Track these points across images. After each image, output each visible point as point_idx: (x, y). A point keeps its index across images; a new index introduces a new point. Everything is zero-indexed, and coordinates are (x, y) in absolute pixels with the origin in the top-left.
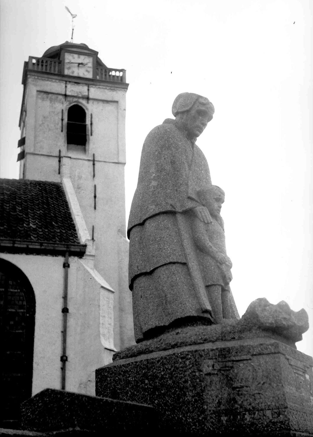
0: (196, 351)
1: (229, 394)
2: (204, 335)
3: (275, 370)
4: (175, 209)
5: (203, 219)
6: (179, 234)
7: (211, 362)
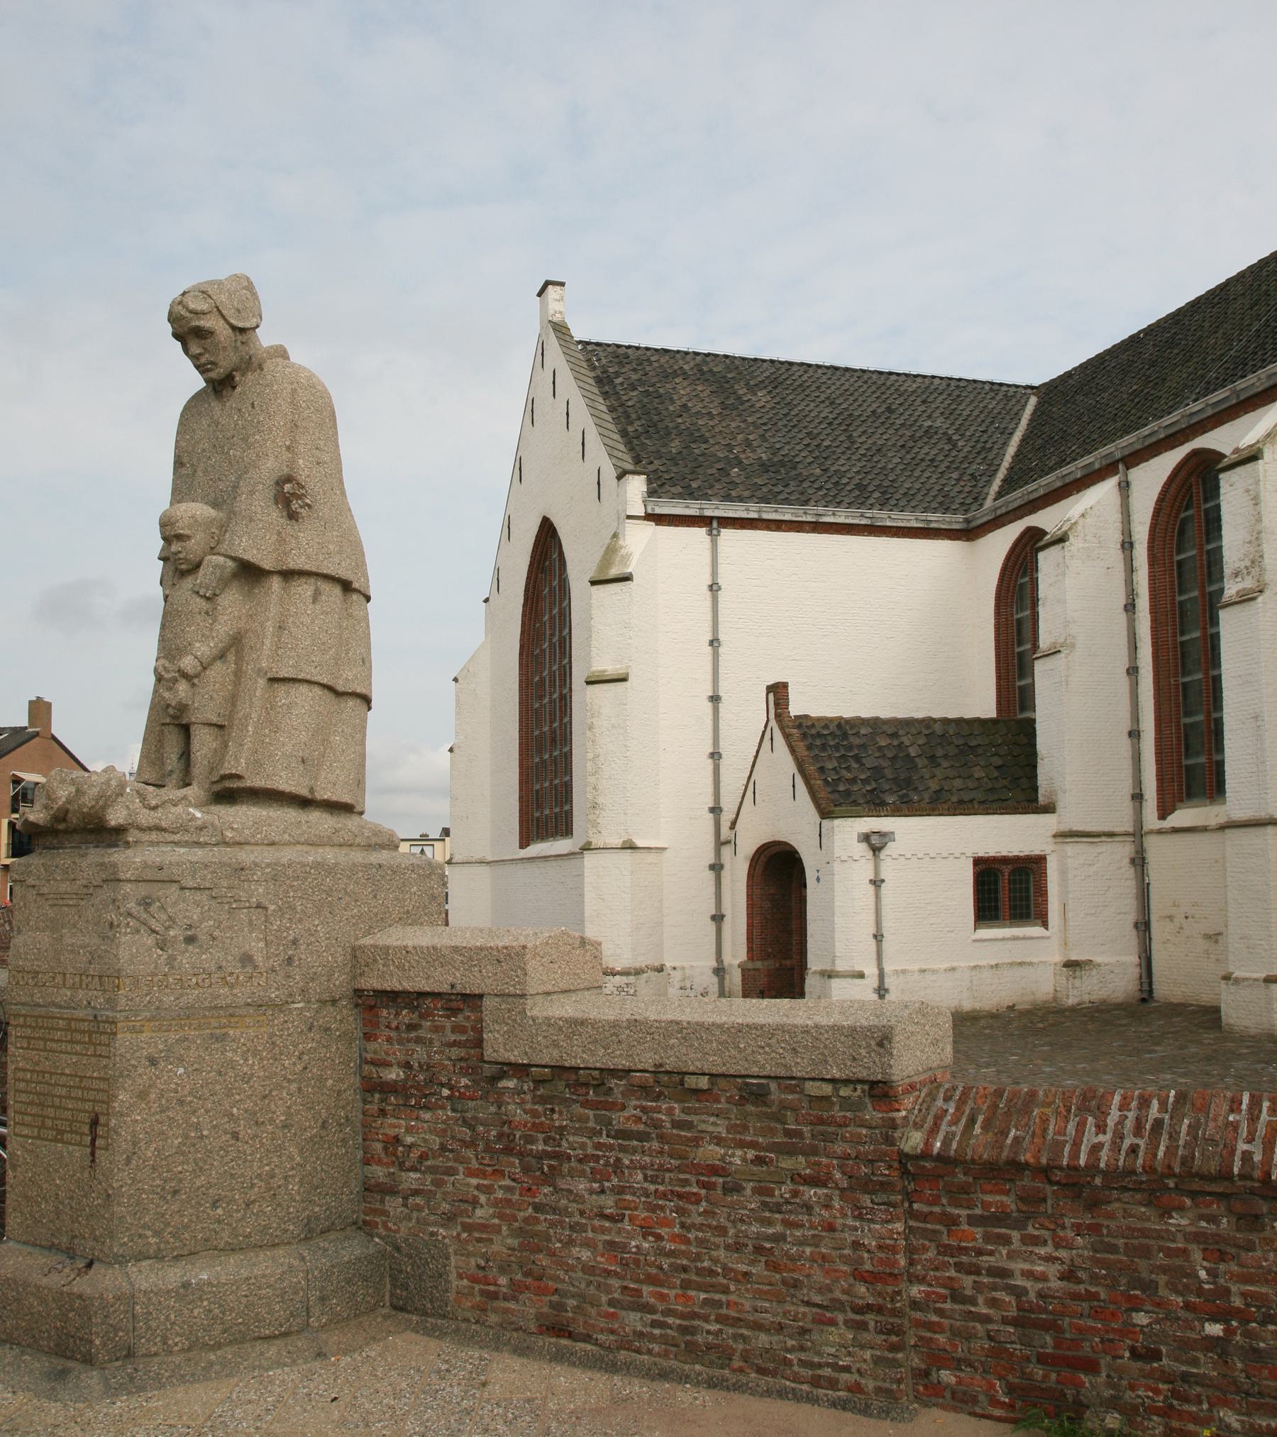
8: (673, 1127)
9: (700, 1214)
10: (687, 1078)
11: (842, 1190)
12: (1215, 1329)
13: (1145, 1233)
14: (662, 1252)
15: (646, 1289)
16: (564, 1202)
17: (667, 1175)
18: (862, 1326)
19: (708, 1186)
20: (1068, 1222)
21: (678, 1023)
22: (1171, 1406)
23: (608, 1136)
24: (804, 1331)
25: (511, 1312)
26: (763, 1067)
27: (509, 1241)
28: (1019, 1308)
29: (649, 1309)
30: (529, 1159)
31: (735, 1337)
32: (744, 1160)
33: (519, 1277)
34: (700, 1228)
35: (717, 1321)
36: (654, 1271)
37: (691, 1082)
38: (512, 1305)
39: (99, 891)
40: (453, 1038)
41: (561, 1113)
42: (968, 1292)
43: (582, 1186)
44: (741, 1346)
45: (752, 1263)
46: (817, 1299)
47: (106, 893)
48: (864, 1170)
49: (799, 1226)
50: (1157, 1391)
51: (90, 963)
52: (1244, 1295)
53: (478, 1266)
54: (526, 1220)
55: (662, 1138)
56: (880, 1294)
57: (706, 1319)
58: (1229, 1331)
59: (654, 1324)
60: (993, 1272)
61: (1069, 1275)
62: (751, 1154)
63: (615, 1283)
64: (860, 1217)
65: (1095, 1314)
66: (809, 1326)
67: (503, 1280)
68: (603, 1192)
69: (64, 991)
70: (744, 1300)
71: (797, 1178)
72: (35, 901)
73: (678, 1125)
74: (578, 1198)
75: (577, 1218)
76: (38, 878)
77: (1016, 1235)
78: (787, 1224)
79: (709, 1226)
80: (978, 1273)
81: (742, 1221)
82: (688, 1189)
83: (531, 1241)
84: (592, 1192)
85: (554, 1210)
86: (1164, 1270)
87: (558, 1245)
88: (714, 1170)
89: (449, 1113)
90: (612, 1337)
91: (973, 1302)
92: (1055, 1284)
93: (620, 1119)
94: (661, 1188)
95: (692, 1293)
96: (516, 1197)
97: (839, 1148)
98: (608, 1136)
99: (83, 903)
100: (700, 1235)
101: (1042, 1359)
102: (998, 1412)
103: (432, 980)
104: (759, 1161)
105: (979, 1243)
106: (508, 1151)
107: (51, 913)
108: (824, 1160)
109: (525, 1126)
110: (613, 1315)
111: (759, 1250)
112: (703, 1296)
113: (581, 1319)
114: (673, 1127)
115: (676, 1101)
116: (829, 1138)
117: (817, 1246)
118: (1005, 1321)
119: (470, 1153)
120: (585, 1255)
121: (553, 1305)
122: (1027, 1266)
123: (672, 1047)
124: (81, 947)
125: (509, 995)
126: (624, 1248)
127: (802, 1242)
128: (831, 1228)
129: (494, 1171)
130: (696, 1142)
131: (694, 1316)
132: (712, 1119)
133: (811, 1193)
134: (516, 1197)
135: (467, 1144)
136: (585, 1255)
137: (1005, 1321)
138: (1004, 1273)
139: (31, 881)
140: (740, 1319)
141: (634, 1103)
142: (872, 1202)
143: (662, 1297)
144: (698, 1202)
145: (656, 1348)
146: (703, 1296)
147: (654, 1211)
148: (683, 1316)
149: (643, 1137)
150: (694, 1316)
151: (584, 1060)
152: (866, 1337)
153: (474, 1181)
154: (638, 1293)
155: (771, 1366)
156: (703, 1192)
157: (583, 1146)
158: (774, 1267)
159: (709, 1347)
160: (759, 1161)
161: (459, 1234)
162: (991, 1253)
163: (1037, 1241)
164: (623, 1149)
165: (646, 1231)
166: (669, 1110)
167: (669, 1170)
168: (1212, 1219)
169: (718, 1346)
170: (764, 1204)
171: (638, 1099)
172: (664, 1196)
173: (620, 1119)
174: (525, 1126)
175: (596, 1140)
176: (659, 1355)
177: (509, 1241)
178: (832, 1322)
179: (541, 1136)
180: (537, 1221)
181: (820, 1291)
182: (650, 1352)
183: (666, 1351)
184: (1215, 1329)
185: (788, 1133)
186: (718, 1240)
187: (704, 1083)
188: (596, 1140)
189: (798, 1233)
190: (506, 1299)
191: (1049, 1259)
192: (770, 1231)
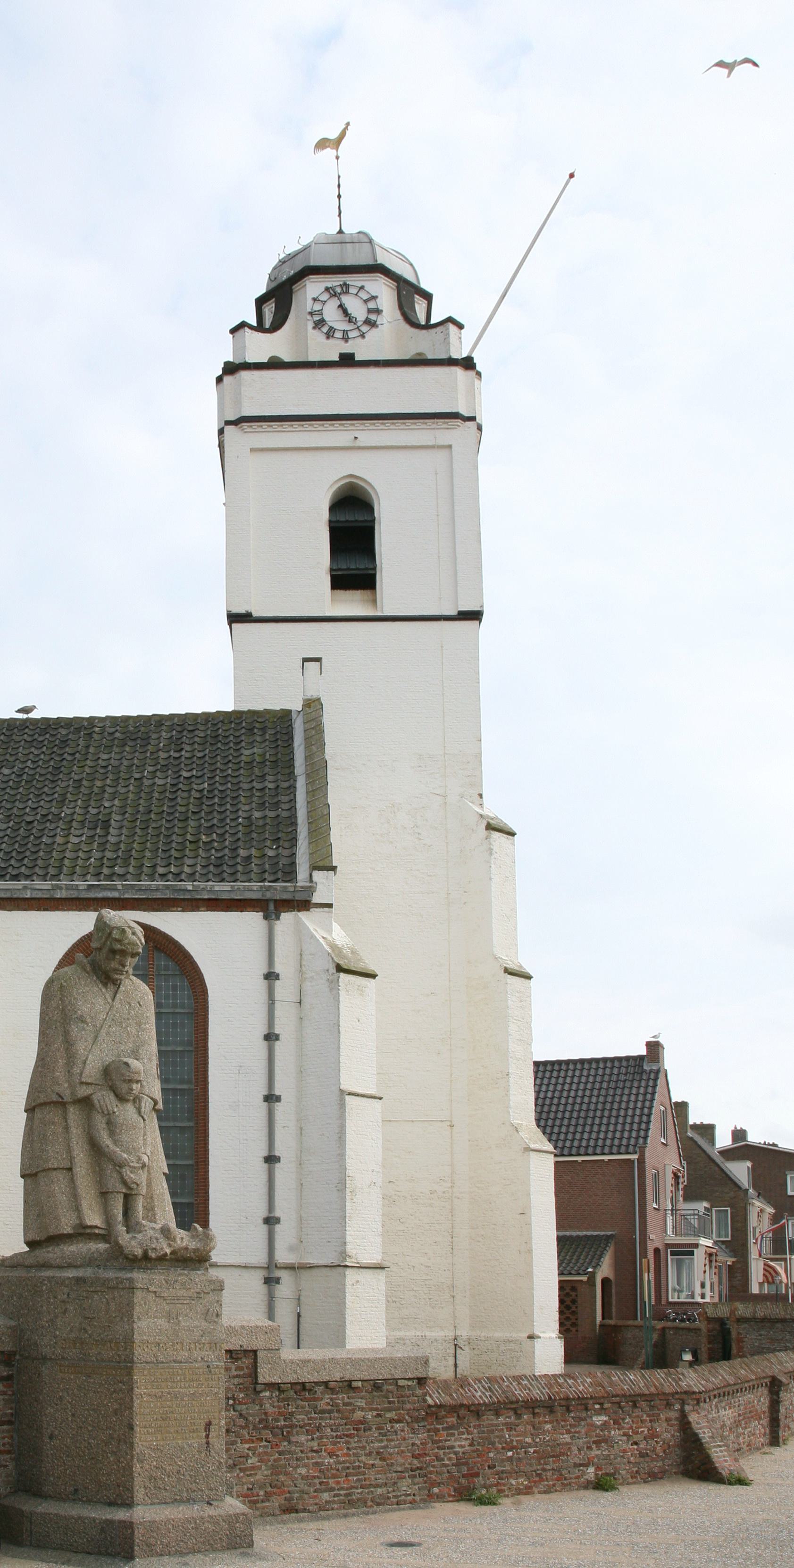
0: (53, 1277)
1: (80, 1324)
2: (69, 1259)
3: (128, 1305)
4: (63, 1099)
5: (102, 1109)
6: (67, 1128)
7: (66, 1290)
8: (344, 1405)
9: (355, 1442)
10: (353, 1383)
11: (408, 1423)
12: (510, 1454)
13: (492, 1425)
14: (339, 1462)
15: (331, 1481)
16: (294, 1448)
17: (341, 1427)
18: (415, 1476)
19: (357, 1430)
20: (472, 1425)
21: (350, 1359)
22: (498, 1483)
23: (315, 1413)
24: (395, 1483)
25: (267, 1507)
26: (384, 1376)
27: (265, 1472)
28: (457, 1459)
29: (332, 1489)
30: (276, 1430)
31: (368, 1493)
32: (372, 1416)
33: (269, 1489)
34: (355, 1448)
35: (361, 1488)
36: (334, 1472)
37: (354, 1384)
38: (267, 1504)
39: (207, 1296)
40: (235, 1373)
41: (292, 1405)
42: (442, 1456)
43: (303, 1438)
44: (370, 1496)
45: (375, 1459)
46: (400, 1469)
47: (212, 1297)
48: (417, 1414)
49: (392, 1440)
50: (495, 1478)
51: (202, 1336)
52: (517, 1441)
53: (248, 1489)
54: (275, 1460)
55: (338, 1411)
56: (422, 1462)
57: (357, 1488)
58: (513, 1454)
59: (335, 1496)
60: (449, 1448)
61: (471, 1445)
62: (375, 1413)
63: (317, 1481)
64: (414, 1433)
65: (479, 1456)
66: (396, 1481)
67: (262, 1493)
68: (313, 1439)
69: (182, 1353)
70: (371, 1475)
71: (392, 1421)
72: (155, 1301)
73: (345, 1404)
74: (302, 1445)
75: (300, 1454)
76: (160, 1287)
77: (456, 1432)
78: (388, 1440)
79: (359, 1447)
80: (444, 1449)
81: (372, 1442)
82: (350, 1432)
83: (276, 1470)
84: (307, 1441)
85: (289, 1452)
86: (497, 1437)
87: (291, 1469)
88: (361, 1422)
89: (232, 1413)
90: (316, 1507)
91: (443, 1460)
92: (467, 1448)
93: (322, 1405)
94: (339, 1434)
95: (350, 1478)
96: (269, 1450)
97: (408, 1406)
98: (315, 1413)
99: (193, 1302)
100: (355, 1451)
101: (464, 1476)
102: (451, 1499)
103: (229, 1344)
104: (379, 1415)
105: (445, 1437)
106: (265, 1427)
107: (167, 1308)
108: (402, 1412)
109: (275, 1413)
110: (315, 1497)
111: (378, 1453)
112: (355, 1478)
113: (301, 1502)
114: (344, 1405)
115: (345, 1394)
116: (404, 1403)
117: (400, 1447)
118: (453, 1465)
119: (245, 1432)
120: (303, 1471)
121: (286, 1499)
122: (459, 1443)
123: (348, 1370)
124: (195, 1327)
125: (272, 1350)
126: (322, 1464)
127: (395, 1447)
128: (404, 1439)
129: (377, 1414)
130: (353, 1411)
131: (352, 1487)
132: (360, 1400)
133: (397, 1426)
134: (269, 1450)
135: (242, 1427)
136: (303, 1471)
137: (453, 1465)
138: (452, 1447)
139: (152, 1289)
140: (371, 1485)
141: (327, 1396)
142: (419, 1426)
143: (338, 1483)
144: (354, 1437)
145: (335, 1506)
146: (355, 1478)
147: (336, 1445)
148: (347, 1489)
149: (330, 1412)
150: (352, 1487)
151: (308, 1378)
152: (417, 1480)
153: (247, 1446)
154: (328, 1483)
155: (383, 1501)
156: (356, 1432)
157: (303, 1420)
158: (383, 1459)
159: (358, 1500)
160: (379, 1415)
161: (238, 1475)
162: (449, 1441)
163: (463, 1433)
164: (321, 1418)
165: (331, 1454)
166: (341, 1398)
167: (342, 1425)
168: (509, 1417)
169: (361, 1498)
170: (380, 1433)
171: (328, 1394)
172: (340, 1437)
173: (322, 1405)
174: (275, 1413)
175: (309, 1416)
176: (337, 1509)
177: (265, 1472)
178: (404, 1477)
179: (282, 1418)
180: (279, 1460)
181: (401, 1466)
182: (333, 1509)
183: (340, 1507)
184: (510, 1454)
185: (390, 1402)
186: (363, 1452)
187: (360, 1384)
188: (309, 1416)
189: (393, 1443)
190: (263, 1501)
191: (466, 1439)
192: (383, 1444)
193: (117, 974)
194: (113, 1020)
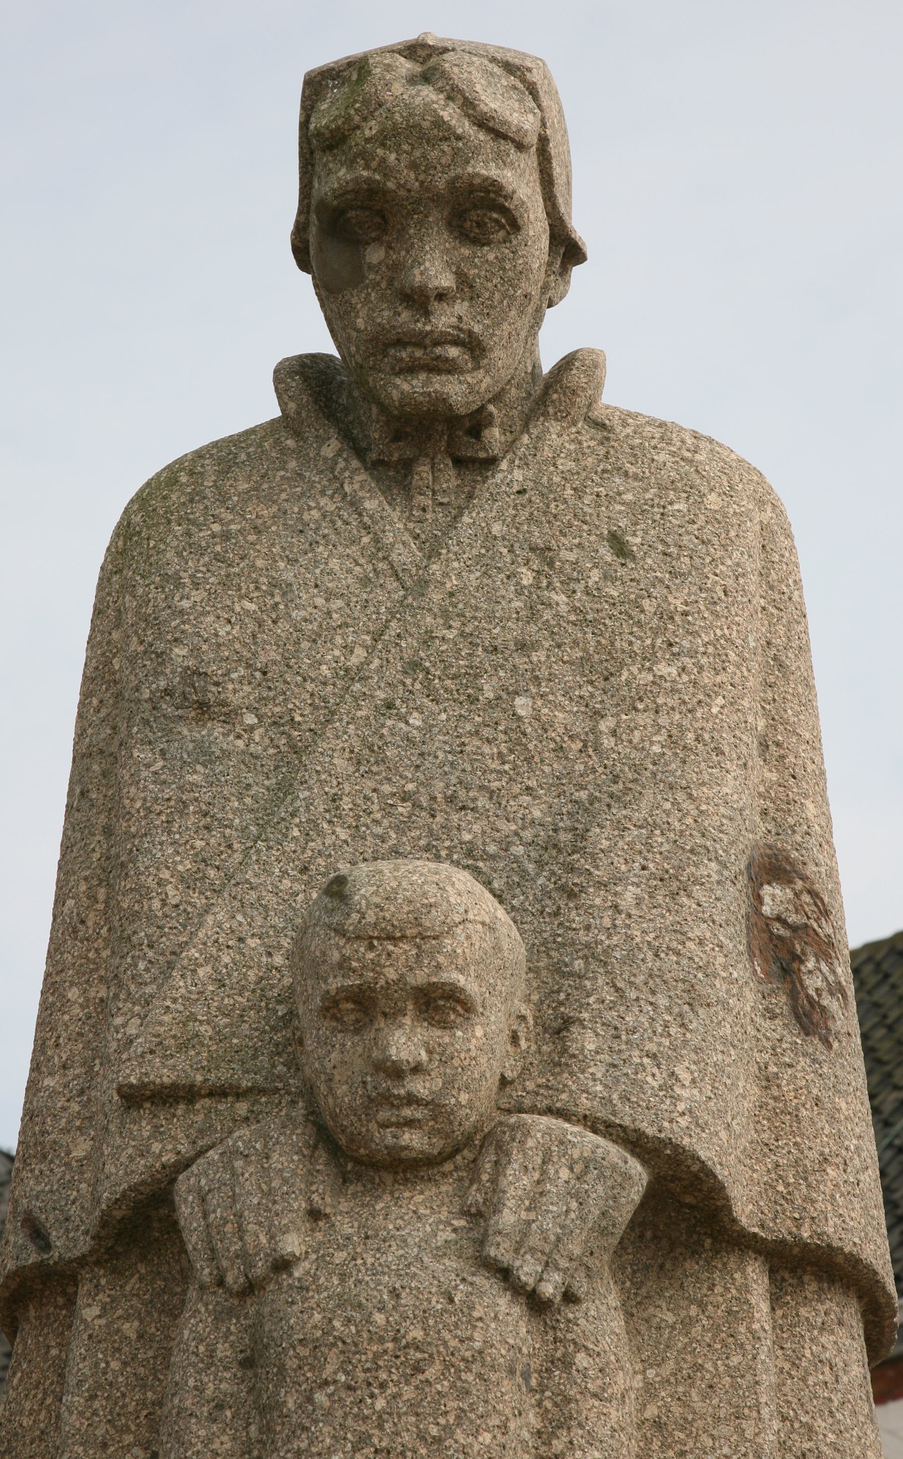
193: (411, 369)
194: (414, 666)
